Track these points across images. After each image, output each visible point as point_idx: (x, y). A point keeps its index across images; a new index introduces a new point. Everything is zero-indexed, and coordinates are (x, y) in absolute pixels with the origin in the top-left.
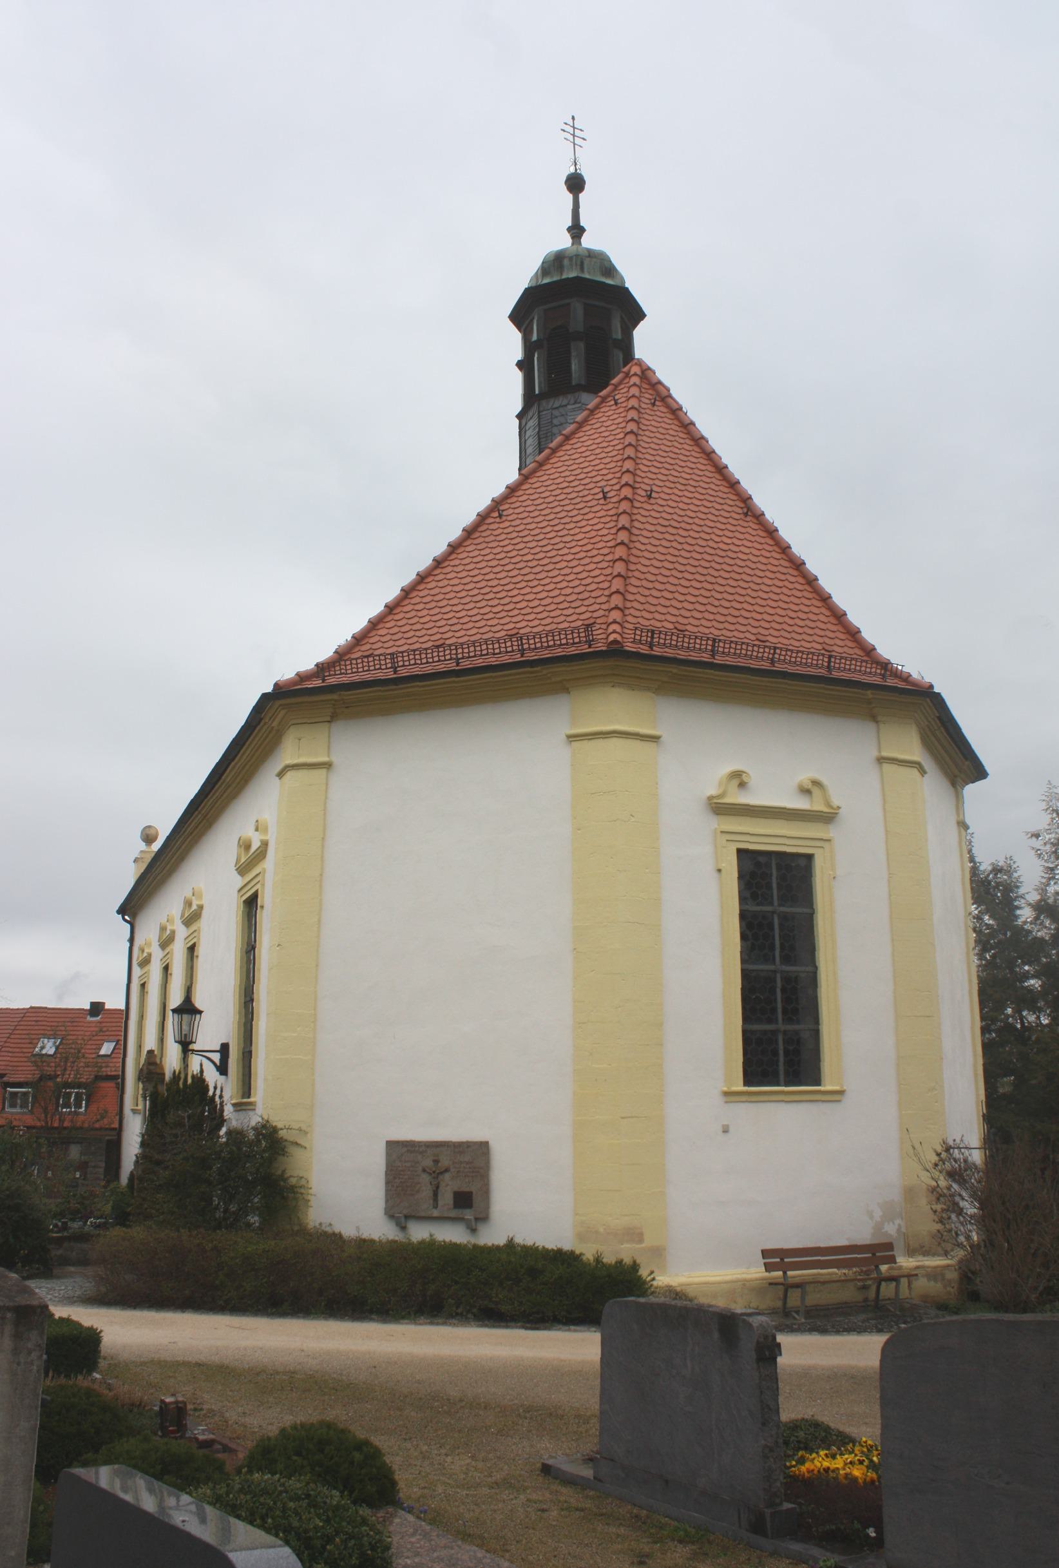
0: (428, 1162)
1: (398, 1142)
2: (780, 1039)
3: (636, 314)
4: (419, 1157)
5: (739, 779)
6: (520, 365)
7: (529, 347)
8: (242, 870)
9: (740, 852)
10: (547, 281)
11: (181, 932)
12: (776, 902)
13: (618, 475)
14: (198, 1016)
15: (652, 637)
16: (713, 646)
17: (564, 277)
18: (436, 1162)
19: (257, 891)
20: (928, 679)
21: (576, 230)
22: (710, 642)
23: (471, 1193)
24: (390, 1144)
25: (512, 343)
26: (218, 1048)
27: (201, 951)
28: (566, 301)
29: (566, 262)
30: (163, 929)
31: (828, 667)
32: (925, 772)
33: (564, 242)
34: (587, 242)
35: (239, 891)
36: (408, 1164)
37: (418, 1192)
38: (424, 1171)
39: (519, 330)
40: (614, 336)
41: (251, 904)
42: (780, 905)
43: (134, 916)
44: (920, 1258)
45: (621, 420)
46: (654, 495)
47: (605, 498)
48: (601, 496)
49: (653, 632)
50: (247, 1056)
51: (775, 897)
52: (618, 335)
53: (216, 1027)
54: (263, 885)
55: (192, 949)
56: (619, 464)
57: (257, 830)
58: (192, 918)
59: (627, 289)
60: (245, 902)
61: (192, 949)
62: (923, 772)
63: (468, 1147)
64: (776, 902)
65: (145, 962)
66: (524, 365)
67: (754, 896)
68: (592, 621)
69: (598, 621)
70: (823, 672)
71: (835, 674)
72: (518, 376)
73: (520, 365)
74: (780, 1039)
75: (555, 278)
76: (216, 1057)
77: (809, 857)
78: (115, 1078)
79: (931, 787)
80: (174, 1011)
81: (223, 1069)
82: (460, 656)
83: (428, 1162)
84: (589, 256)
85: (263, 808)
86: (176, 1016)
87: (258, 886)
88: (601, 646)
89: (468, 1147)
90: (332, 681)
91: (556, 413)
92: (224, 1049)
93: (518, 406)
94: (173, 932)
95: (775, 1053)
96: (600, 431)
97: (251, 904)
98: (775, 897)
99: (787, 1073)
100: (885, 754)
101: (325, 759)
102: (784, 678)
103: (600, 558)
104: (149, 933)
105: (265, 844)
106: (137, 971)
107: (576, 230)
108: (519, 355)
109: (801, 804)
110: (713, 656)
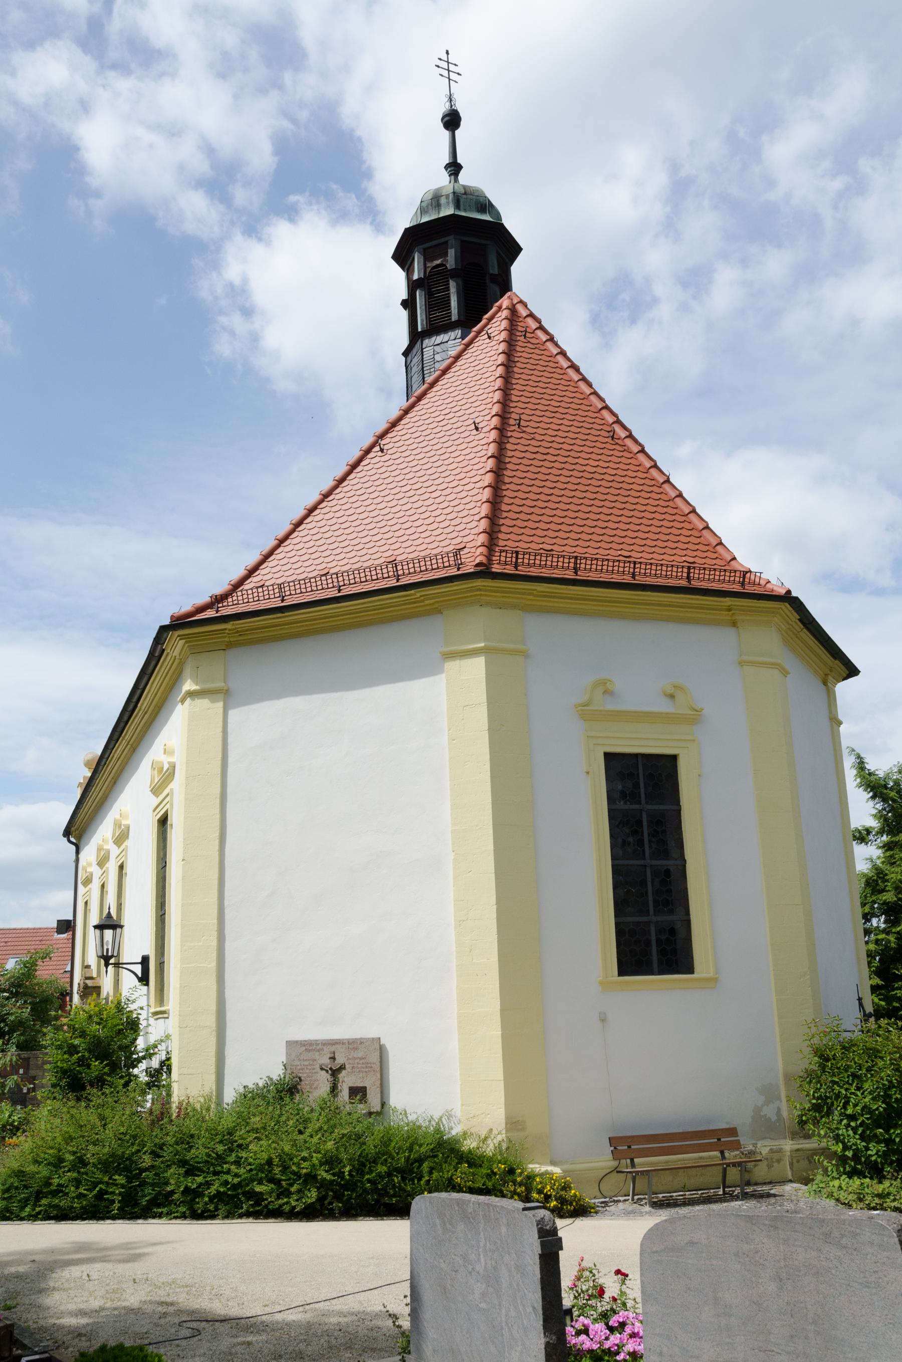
0: (325, 1060)
1: (297, 1042)
2: (653, 929)
3: (512, 249)
4: (317, 1054)
5: (605, 689)
6: (405, 304)
7: (413, 286)
8: (156, 790)
9: (608, 756)
10: (425, 219)
11: (114, 851)
12: (644, 803)
13: (490, 406)
14: (118, 930)
15: (517, 558)
16: (576, 563)
17: (441, 215)
18: (333, 1058)
19: (167, 811)
20: (788, 585)
21: (454, 168)
22: (572, 560)
23: (365, 1088)
24: (289, 1044)
25: (396, 282)
26: (140, 960)
27: (128, 869)
28: (443, 240)
29: (443, 200)
30: (100, 849)
31: (688, 577)
32: (788, 673)
33: (443, 180)
34: (464, 178)
35: (154, 811)
36: (306, 1063)
37: (316, 1088)
38: (322, 1069)
39: (403, 270)
40: (491, 272)
41: (163, 822)
42: (647, 803)
43: (79, 837)
44: (802, 1141)
45: (493, 353)
46: (523, 423)
47: (477, 429)
48: (473, 427)
49: (517, 553)
50: (161, 965)
51: (643, 796)
52: (494, 270)
53: (136, 942)
54: (172, 805)
55: (121, 867)
56: (490, 395)
57: (165, 753)
58: (121, 837)
59: (502, 224)
60: (159, 821)
61: (121, 867)
62: (785, 673)
63: (361, 1043)
64: (644, 803)
65: (88, 881)
66: (408, 304)
67: (624, 796)
68: (462, 545)
69: (468, 545)
70: (684, 583)
71: (695, 584)
72: (403, 315)
73: (405, 304)
74: (653, 929)
75: (434, 217)
76: (138, 969)
77: (674, 758)
78: (725, 1171)
79: (800, 680)
80: (96, 927)
81: (144, 979)
82: (341, 583)
83: (325, 1060)
84: (465, 194)
85: (177, 733)
86: (98, 931)
87: (168, 806)
88: (469, 569)
89: (361, 1043)
90: (224, 612)
91: (438, 349)
92: (145, 961)
93: (405, 342)
94: (108, 852)
95: (648, 943)
96: (479, 361)
97: (163, 822)
98: (643, 796)
99: (660, 963)
100: (745, 658)
101: (220, 684)
102: (643, 590)
103: (471, 486)
104: (89, 854)
105: (173, 767)
106: (81, 889)
107: (454, 168)
108: (404, 295)
109: (663, 706)
110: (576, 573)
